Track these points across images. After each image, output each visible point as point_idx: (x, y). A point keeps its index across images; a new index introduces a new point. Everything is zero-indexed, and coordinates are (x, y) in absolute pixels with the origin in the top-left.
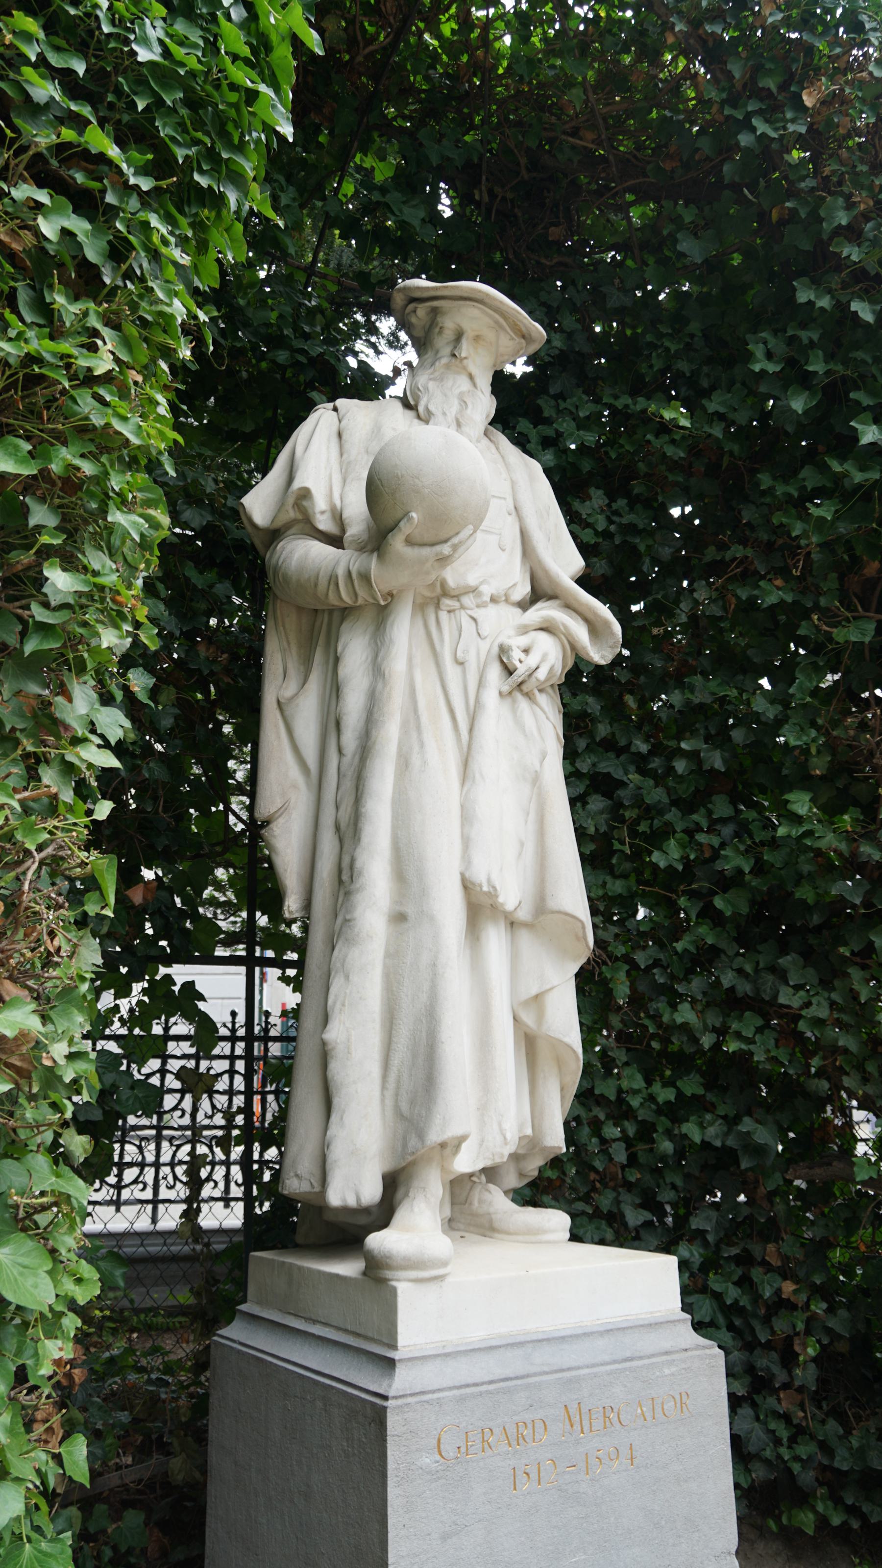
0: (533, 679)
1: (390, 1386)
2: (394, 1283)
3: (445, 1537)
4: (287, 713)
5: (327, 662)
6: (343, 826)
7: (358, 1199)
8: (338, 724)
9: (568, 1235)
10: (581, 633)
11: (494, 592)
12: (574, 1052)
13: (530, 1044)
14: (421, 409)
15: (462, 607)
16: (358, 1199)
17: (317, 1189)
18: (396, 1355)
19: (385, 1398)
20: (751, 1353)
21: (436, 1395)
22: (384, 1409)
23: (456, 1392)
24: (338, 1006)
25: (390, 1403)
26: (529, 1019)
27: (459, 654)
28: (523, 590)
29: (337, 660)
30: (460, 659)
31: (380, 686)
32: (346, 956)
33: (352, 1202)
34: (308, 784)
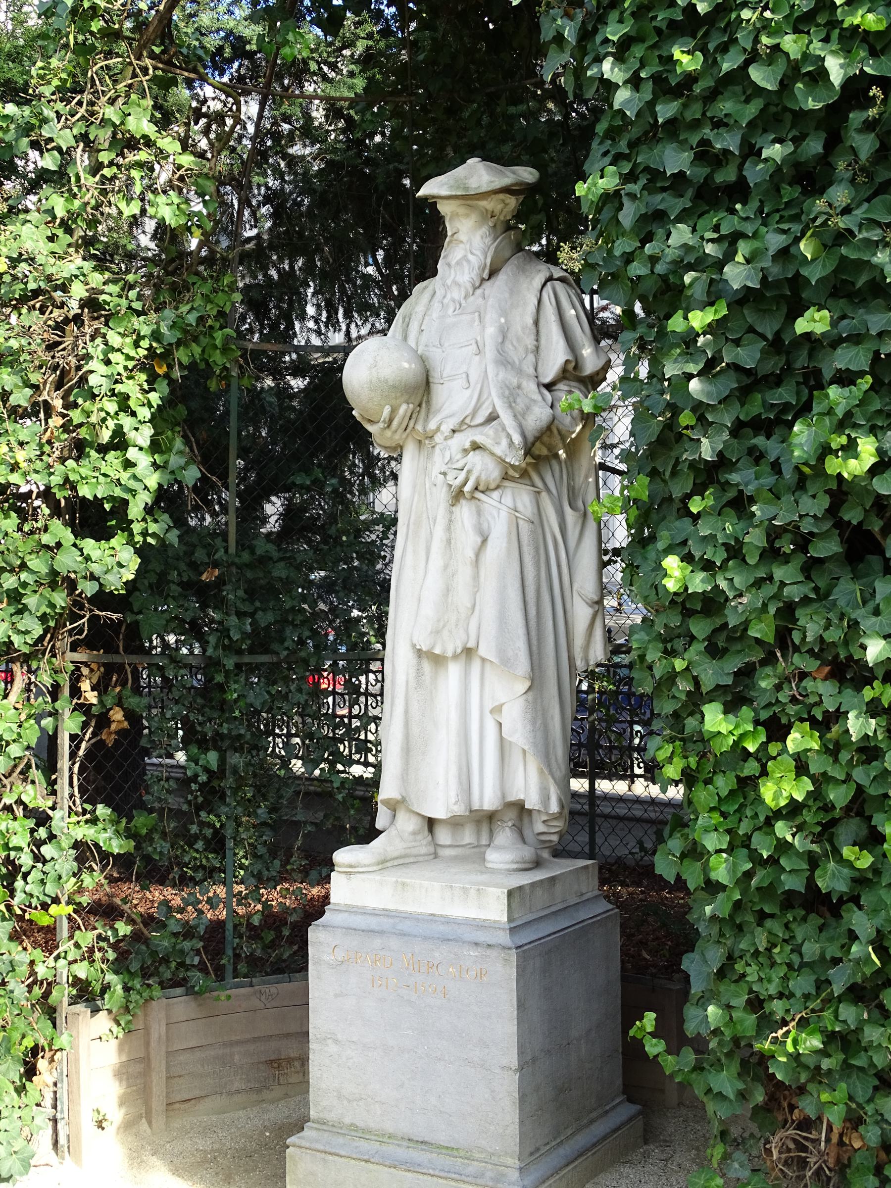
3: (336, 996)
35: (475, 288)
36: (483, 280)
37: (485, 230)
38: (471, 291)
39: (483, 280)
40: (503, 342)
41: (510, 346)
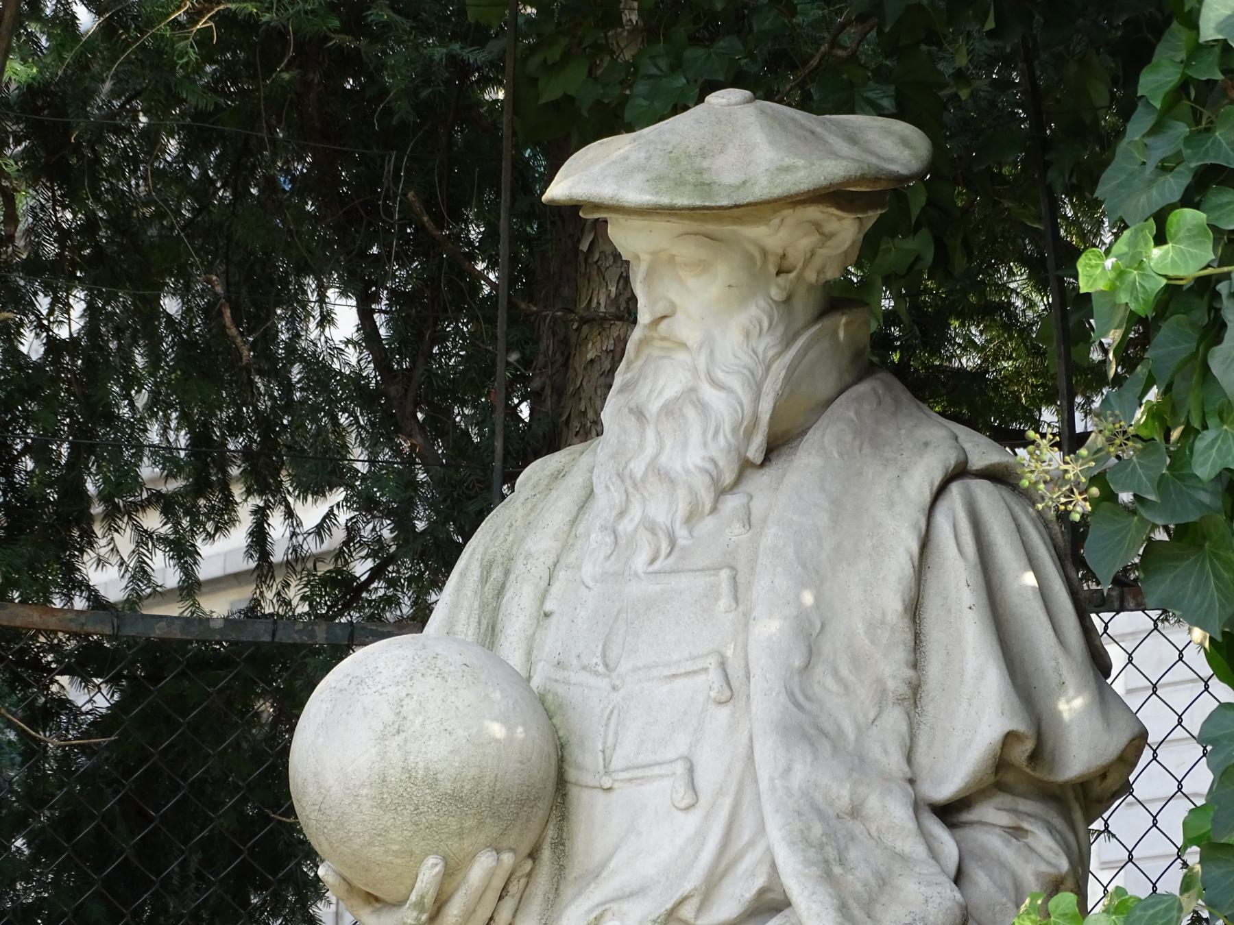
35: (721, 492)
36: (745, 467)
37: (756, 311)
38: (707, 498)
39: (745, 467)
40: (807, 667)
41: (830, 682)
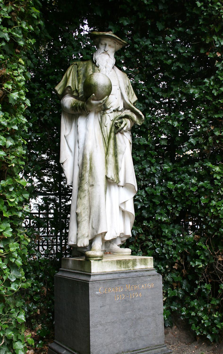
0: (123, 130)
1: (90, 279)
2: (91, 261)
3: (101, 307)
4: (67, 138)
5: (75, 126)
6: (80, 165)
7: (84, 245)
8: (78, 141)
9: (130, 253)
10: (135, 117)
11: (114, 109)
12: (133, 215)
13: (124, 213)
14: (97, 64)
15: (106, 113)
16: (84, 245)
17: (75, 244)
18: (91, 274)
19: (89, 281)
20: (132, 243)
21: (99, 281)
22: (89, 283)
23: (104, 281)
24: (79, 205)
25: (89, 282)
26: (123, 207)
27: (106, 124)
28: (121, 107)
29: (78, 126)
30: (106, 126)
31: (87, 133)
32: (80, 194)
33: (82, 246)
34: (72, 155)
